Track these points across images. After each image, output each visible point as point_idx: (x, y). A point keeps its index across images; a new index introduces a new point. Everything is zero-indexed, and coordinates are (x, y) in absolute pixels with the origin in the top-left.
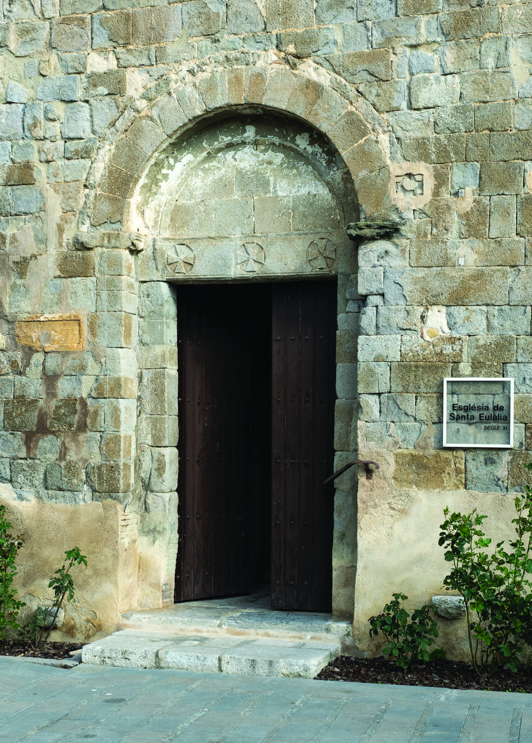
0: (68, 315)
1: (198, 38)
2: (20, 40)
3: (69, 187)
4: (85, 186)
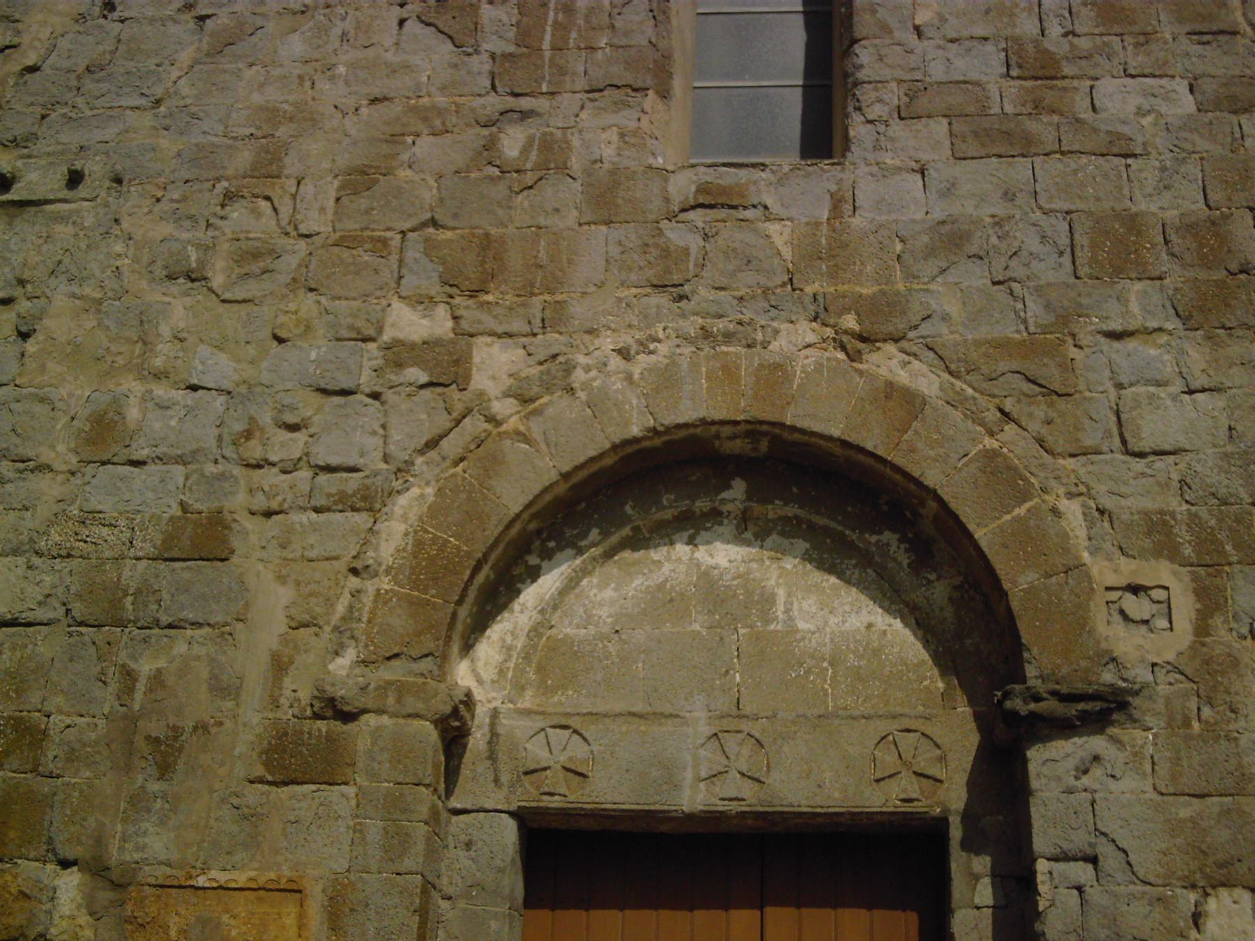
0: (272, 875)
1: (639, 290)
2: (237, 270)
3: (314, 570)
4: (354, 571)
